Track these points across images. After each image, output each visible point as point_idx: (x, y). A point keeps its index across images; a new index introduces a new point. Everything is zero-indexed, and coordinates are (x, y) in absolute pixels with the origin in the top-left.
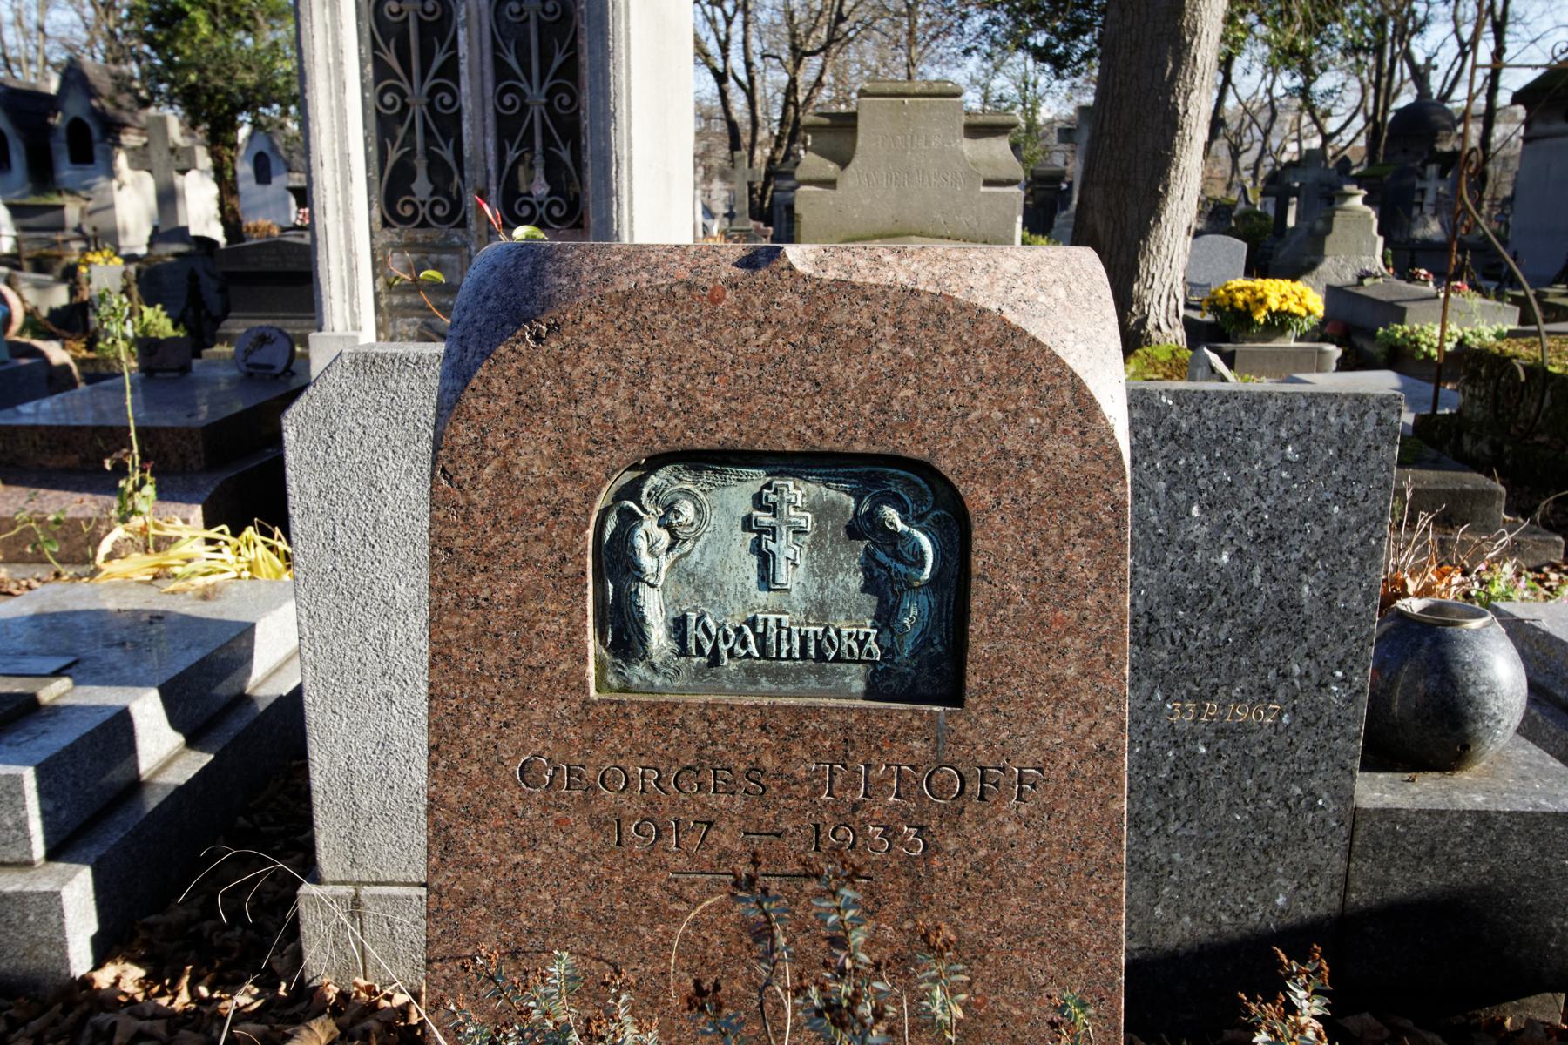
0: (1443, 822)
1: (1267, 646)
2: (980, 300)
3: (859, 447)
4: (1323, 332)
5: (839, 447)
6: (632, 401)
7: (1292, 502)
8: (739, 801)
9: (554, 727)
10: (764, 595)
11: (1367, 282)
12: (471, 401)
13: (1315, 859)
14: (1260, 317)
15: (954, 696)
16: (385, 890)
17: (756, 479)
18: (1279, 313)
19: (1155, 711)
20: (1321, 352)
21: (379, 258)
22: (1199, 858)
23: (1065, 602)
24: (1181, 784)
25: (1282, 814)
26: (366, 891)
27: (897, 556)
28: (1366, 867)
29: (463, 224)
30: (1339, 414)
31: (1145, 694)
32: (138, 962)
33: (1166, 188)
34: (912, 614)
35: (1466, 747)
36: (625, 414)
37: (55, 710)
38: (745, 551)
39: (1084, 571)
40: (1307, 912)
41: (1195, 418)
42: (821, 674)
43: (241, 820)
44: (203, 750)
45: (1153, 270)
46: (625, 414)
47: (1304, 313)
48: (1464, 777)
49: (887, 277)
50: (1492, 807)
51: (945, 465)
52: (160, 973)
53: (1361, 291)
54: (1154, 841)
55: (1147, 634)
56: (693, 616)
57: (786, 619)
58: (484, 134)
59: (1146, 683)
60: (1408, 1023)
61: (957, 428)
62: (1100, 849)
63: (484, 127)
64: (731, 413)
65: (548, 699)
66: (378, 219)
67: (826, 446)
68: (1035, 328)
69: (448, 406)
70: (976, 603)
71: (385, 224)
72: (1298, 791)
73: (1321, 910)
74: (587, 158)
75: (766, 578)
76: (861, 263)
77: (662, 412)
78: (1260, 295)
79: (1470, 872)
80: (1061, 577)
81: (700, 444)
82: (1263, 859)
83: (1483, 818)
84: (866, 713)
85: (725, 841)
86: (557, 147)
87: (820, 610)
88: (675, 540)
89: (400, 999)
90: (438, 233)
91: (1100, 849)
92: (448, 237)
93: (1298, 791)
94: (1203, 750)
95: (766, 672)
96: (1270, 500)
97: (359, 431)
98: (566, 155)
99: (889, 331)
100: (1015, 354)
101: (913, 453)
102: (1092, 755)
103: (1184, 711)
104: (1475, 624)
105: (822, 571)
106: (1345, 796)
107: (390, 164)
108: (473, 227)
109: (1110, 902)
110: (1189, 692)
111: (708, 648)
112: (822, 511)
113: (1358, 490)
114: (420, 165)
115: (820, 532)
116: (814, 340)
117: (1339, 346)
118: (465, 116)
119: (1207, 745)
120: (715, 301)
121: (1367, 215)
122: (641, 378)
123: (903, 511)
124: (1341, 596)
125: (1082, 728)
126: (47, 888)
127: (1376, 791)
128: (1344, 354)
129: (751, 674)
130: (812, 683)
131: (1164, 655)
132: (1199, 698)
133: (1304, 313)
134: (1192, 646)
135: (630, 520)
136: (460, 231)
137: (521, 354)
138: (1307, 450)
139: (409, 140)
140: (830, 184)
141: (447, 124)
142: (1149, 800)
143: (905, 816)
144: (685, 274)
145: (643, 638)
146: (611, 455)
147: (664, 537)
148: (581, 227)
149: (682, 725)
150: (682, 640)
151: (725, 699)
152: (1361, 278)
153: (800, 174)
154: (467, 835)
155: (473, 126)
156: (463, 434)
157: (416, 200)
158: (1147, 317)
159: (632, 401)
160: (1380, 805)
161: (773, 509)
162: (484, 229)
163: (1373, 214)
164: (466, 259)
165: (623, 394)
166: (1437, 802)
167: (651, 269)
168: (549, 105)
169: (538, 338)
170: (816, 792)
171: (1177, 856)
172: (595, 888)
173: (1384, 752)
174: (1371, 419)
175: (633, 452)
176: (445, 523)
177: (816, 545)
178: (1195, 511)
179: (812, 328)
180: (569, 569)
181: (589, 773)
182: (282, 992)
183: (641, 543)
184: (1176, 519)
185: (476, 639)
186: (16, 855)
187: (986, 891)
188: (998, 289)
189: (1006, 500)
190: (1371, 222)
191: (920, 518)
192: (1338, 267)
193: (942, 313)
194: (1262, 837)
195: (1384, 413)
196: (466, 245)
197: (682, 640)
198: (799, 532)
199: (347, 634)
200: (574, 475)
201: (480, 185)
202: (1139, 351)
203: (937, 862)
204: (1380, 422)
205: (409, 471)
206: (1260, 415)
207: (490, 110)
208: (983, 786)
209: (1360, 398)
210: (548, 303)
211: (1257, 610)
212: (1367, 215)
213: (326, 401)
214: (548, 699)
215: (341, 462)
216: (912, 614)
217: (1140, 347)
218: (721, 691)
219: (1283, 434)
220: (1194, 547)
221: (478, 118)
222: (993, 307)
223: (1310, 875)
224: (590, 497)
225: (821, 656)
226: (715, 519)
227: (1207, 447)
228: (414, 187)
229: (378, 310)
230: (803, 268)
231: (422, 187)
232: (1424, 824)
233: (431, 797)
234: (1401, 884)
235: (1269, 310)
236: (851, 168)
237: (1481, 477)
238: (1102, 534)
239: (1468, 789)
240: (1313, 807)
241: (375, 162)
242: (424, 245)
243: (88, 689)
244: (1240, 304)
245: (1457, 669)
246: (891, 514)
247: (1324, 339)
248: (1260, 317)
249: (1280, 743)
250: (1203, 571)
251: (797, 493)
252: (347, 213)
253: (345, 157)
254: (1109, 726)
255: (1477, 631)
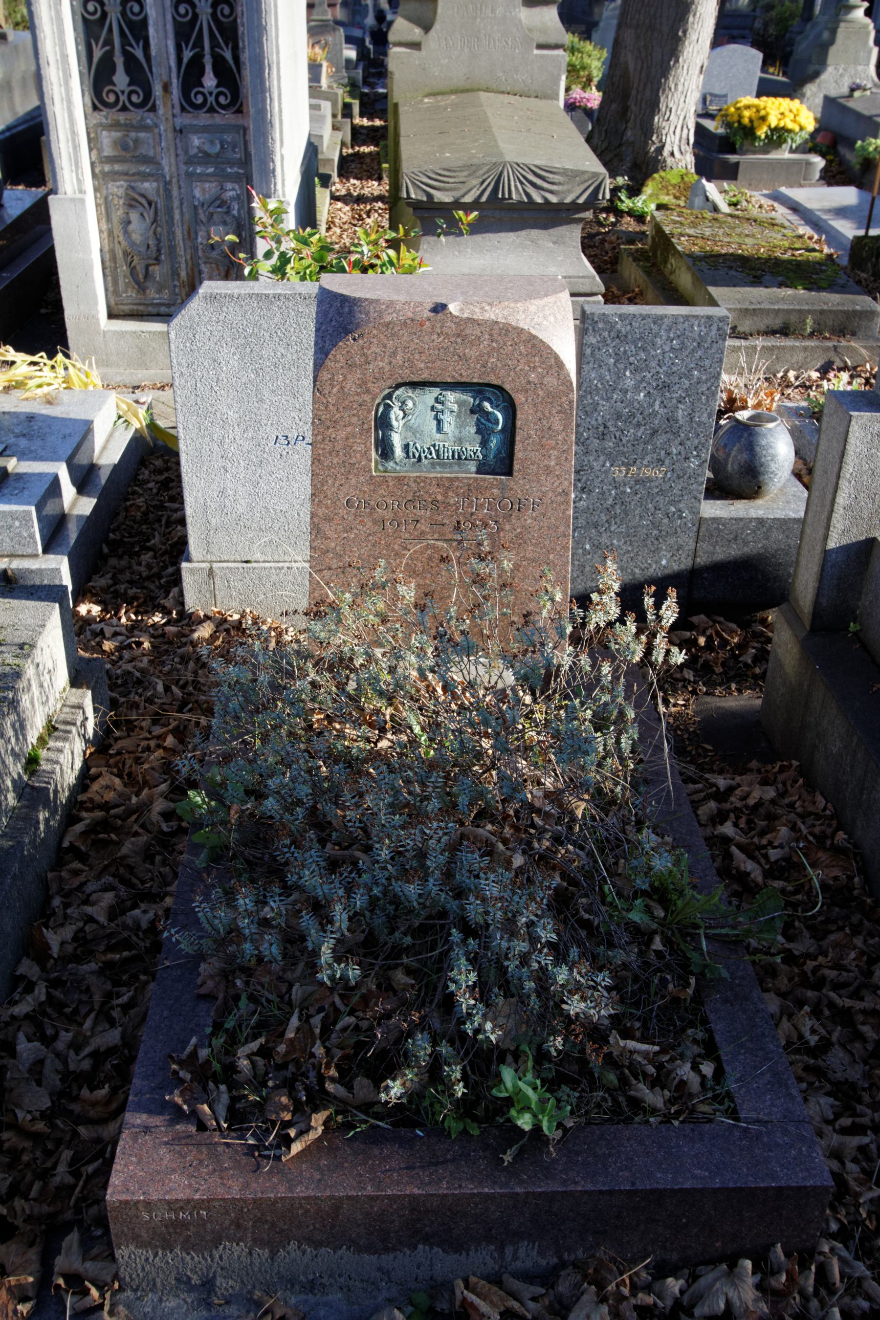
0: (741, 524)
1: (660, 439)
2: (522, 325)
3: (475, 380)
4: (812, 145)
5: (468, 380)
6: (390, 363)
7: (675, 369)
8: (428, 513)
9: (359, 486)
10: (438, 435)
11: (857, 94)
12: (328, 363)
13: (681, 542)
14: (762, 132)
15: (509, 473)
16: (225, 565)
17: (436, 391)
18: (776, 129)
19: (606, 472)
20: (808, 164)
21: (92, 135)
22: (625, 542)
23: (550, 438)
24: (617, 507)
25: (666, 521)
26: (215, 565)
27: (489, 420)
28: (704, 545)
29: (153, 109)
30: (699, 326)
31: (601, 463)
32: (97, 603)
33: (685, 32)
34: (494, 442)
35: (759, 487)
36: (387, 368)
37: (19, 477)
38: (431, 419)
39: (557, 426)
40: (676, 567)
41: (629, 327)
42: (459, 465)
43: (111, 535)
44: (89, 496)
45: (671, 105)
46: (387, 368)
47: (797, 129)
48: (759, 502)
49: (486, 316)
50: (765, 516)
51: (507, 387)
52: (110, 604)
53: (851, 104)
54: (604, 535)
55: (603, 434)
56: (411, 444)
57: (446, 444)
58: (166, 38)
59: (602, 458)
60: (722, 619)
61: (512, 373)
62: (562, 528)
63: (166, 31)
64: (427, 367)
65: (357, 475)
66: (90, 104)
67: (463, 380)
68: (541, 336)
69: (318, 366)
70: (518, 438)
71: (95, 108)
72: (673, 509)
73: (683, 567)
74: (245, 56)
75: (439, 429)
76: (477, 310)
77: (401, 367)
78: (763, 113)
79: (753, 547)
80: (550, 429)
81: (416, 380)
82: (656, 542)
83: (761, 521)
84: (476, 479)
85: (423, 528)
86: (222, 49)
87: (459, 441)
88: (405, 415)
89: (236, 617)
90: (135, 115)
91: (562, 528)
92: (142, 119)
93: (673, 509)
94: (629, 490)
95: (439, 464)
96: (665, 368)
97: (208, 333)
98: (228, 55)
99: (487, 337)
100: (534, 346)
101: (495, 382)
102: (559, 494)
103: (620, 471)
104: (771, 425)
105: (461, 426)
106: (695, 512)
107: (95, 60)
108: (161, 111)
109: (565, 548)
110: (623, 463)
111: (417, 455)
112: (461, 404)
113: (707, 363)
114: (119, 60)
115: (460, 412)
116: (459, 340)
117: (823, 156)
118: (151, 22)
119: (631, 488)
120: (422, 325)
121: (866, 26)
122: (394, 354)
123: (491, 403)
124: (697, 415)
125: (556, 484)
126: (53, 566)
127: (713, 509)
128: (829, 163)
129: (433, 465)
130: (456, 468)
131: (611, 444)
132: (628, 465)
133: (797, 129)
134: (624, 439)
135: (388, 407)
136: (151, 114)
137: (348, 347)
138: (683, 343)
139: (109, 42)
140: (416, 46)
141: (137, 29)
142: (602, 515)
143: (490, 517)
144: (411, 315)
145: (393, 452)
146: (383, 384)
147: (401, 414)
148: (241, 112)
149: (408, 485)
150: (407, 453)
151: (424, 475)
152: (852, 90)
153: (392, 37)
154: (325, 527)
155: (157, 31)
156: (325, 375)
157: (116, 89)
158: (663, 146)
159: (390, 363)
160: (713, 516)
161: (442, 403)
162: (170, 113)
163: (872, 26)
164: (157, 137)
165: (386, 361)
166: (741, 514)
167: (398, 312)
168: (214, 15)
169: (354, 339)
170: (457, 509)
171: (615, 542)
172: (374, 546)
173: (718, 489)
174: (714, 328)
175: (390, 382)
176: (318, 409)
177: (458, 416)
178: (628, 373)
179: (459, 336)
180: (366, 426)
181: (372, 503)
182: (174, 616)
183: (393, 416)
184: (619, 378)
185: (330, 453)
186: (30, 551)
187: (520, 544)
188: (528, 320)
189: (530, 400)
190: (868, 34)
191: (497, 406)
192: (833, 80)
193: (507, 330)
194: (656, 532)
195: (721, 325)
196: (157, 126)
197: (407, 453)
198: (452, 412)
199: (203, 437)
200: (368, 391)
201: (165, 78)
202: (655, 175)
203: (502, 534)
204: (719, 329)
205: (234, 354)
206: (660, 326)
207: (169, 17)
208: (520, 506)
209: (709, 318)
210: (358, 326)
211: (656, 422)
212: (866, 26)
213: (191, 318)
214: (357, 475)
215: (199, 349)
216: (494, 442)
217: (657, 171)
218: (421, 471)
219: (672, 335)
220: (626, 391)
221: (161, 24)
222: (526, 327)
223: (678, 550)
224: (373, 399)
225: (460, 458)
226: (420, 407)
227: (635, 342)
228: (115, 79)
229: (94, 175)
230: (455, 313)
231: (121, 79)
232: (733, 525)
233: (312, 513)
234: (722, 553)
235: (769, 126)
236: (432, 32)
237: (868, 299)
238: (565, 412)
239: (758, 508)
240: (680, 517)
241: (84, 59)
242: (126, 125)
243: (27, 463)
244: (746, 121)
245: (757, 449)
246: (487, 405)
247: (810, 151)
248: (762, 132)
249: (665, 487)
250: (631, 403)
251: (451, 397)
252: (69, 102)
253: (65, 57)
254: (566, 483)
255: (770, 429)
